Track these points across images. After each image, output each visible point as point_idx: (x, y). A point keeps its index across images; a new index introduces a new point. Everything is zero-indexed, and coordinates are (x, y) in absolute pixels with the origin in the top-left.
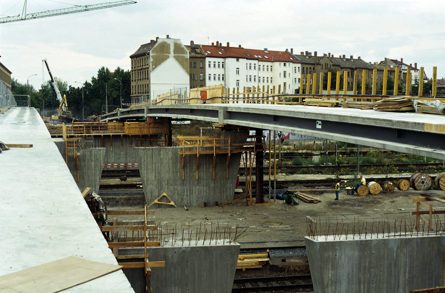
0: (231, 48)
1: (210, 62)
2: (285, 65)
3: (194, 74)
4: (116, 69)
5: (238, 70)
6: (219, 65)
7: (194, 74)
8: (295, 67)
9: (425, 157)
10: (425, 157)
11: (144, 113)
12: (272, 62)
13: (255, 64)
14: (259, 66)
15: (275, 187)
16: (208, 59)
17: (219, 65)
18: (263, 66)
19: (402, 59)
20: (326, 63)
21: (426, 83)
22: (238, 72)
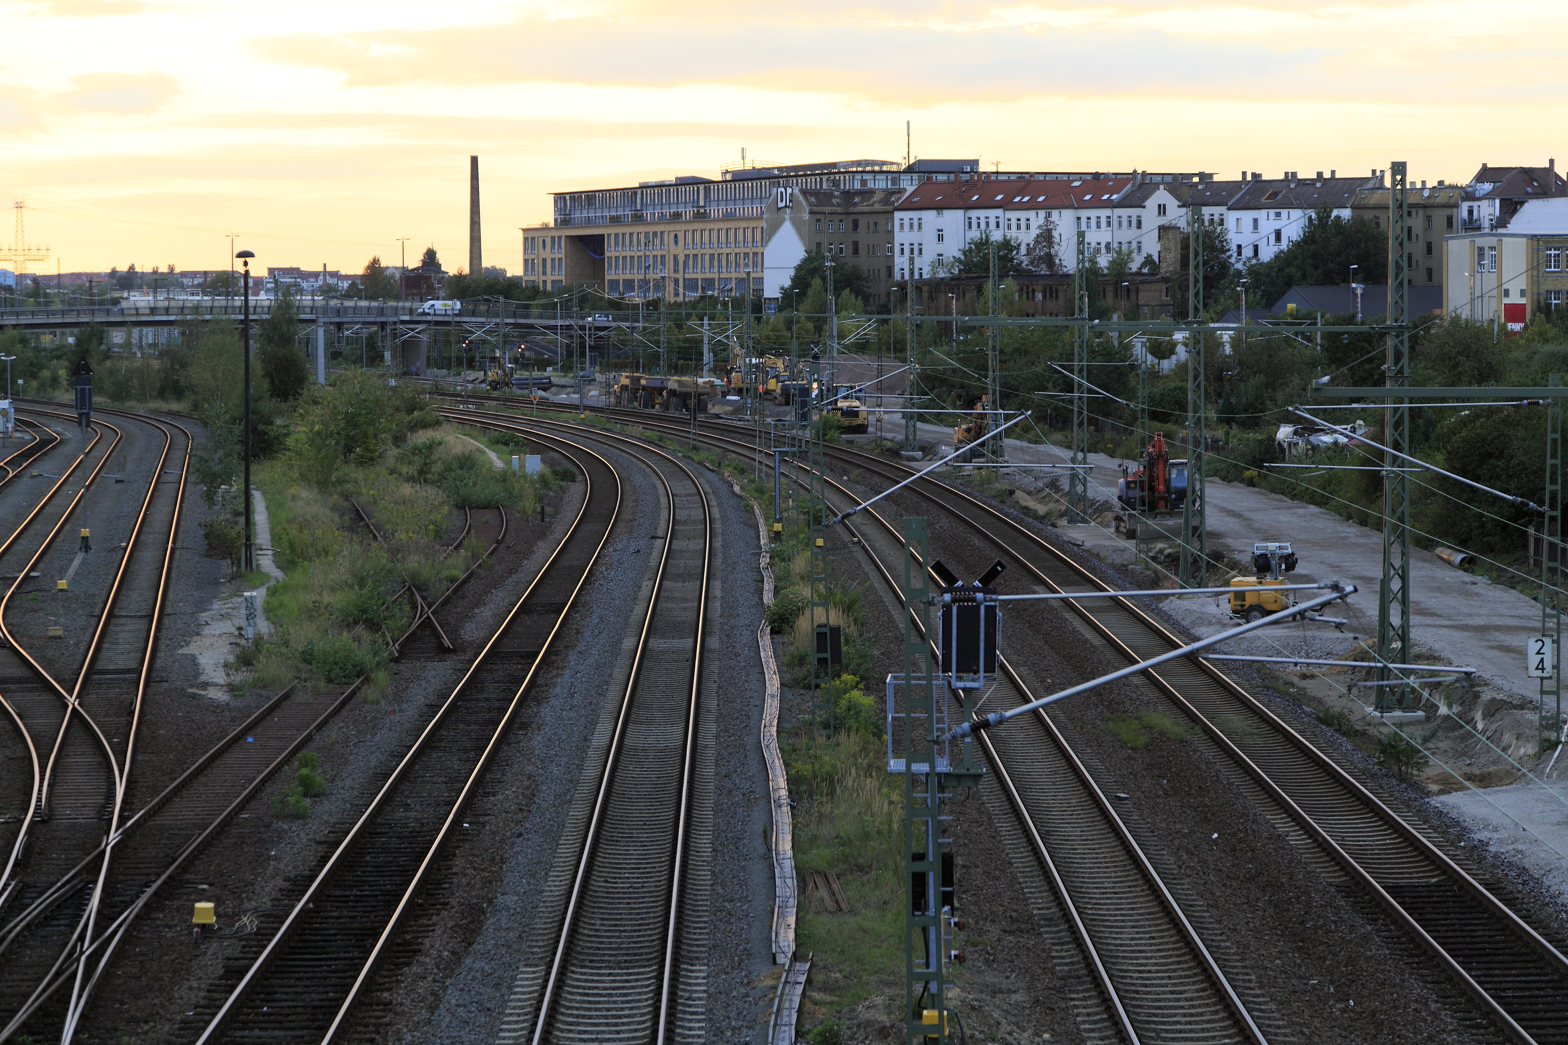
0: (1265, 181)
2: (1278, 215)
5: (1486, 250)
6: (911, 225)
8: (1019, 220)
9: (1041, 710)
10: (1041, 710)
11: (1550, 560)
13: (997, 217)
14: (1009, 220)
16: (898, 215)
17: (911, 225)
18: (1089, 218)
19: (1552, 161)
22: (940, 238)
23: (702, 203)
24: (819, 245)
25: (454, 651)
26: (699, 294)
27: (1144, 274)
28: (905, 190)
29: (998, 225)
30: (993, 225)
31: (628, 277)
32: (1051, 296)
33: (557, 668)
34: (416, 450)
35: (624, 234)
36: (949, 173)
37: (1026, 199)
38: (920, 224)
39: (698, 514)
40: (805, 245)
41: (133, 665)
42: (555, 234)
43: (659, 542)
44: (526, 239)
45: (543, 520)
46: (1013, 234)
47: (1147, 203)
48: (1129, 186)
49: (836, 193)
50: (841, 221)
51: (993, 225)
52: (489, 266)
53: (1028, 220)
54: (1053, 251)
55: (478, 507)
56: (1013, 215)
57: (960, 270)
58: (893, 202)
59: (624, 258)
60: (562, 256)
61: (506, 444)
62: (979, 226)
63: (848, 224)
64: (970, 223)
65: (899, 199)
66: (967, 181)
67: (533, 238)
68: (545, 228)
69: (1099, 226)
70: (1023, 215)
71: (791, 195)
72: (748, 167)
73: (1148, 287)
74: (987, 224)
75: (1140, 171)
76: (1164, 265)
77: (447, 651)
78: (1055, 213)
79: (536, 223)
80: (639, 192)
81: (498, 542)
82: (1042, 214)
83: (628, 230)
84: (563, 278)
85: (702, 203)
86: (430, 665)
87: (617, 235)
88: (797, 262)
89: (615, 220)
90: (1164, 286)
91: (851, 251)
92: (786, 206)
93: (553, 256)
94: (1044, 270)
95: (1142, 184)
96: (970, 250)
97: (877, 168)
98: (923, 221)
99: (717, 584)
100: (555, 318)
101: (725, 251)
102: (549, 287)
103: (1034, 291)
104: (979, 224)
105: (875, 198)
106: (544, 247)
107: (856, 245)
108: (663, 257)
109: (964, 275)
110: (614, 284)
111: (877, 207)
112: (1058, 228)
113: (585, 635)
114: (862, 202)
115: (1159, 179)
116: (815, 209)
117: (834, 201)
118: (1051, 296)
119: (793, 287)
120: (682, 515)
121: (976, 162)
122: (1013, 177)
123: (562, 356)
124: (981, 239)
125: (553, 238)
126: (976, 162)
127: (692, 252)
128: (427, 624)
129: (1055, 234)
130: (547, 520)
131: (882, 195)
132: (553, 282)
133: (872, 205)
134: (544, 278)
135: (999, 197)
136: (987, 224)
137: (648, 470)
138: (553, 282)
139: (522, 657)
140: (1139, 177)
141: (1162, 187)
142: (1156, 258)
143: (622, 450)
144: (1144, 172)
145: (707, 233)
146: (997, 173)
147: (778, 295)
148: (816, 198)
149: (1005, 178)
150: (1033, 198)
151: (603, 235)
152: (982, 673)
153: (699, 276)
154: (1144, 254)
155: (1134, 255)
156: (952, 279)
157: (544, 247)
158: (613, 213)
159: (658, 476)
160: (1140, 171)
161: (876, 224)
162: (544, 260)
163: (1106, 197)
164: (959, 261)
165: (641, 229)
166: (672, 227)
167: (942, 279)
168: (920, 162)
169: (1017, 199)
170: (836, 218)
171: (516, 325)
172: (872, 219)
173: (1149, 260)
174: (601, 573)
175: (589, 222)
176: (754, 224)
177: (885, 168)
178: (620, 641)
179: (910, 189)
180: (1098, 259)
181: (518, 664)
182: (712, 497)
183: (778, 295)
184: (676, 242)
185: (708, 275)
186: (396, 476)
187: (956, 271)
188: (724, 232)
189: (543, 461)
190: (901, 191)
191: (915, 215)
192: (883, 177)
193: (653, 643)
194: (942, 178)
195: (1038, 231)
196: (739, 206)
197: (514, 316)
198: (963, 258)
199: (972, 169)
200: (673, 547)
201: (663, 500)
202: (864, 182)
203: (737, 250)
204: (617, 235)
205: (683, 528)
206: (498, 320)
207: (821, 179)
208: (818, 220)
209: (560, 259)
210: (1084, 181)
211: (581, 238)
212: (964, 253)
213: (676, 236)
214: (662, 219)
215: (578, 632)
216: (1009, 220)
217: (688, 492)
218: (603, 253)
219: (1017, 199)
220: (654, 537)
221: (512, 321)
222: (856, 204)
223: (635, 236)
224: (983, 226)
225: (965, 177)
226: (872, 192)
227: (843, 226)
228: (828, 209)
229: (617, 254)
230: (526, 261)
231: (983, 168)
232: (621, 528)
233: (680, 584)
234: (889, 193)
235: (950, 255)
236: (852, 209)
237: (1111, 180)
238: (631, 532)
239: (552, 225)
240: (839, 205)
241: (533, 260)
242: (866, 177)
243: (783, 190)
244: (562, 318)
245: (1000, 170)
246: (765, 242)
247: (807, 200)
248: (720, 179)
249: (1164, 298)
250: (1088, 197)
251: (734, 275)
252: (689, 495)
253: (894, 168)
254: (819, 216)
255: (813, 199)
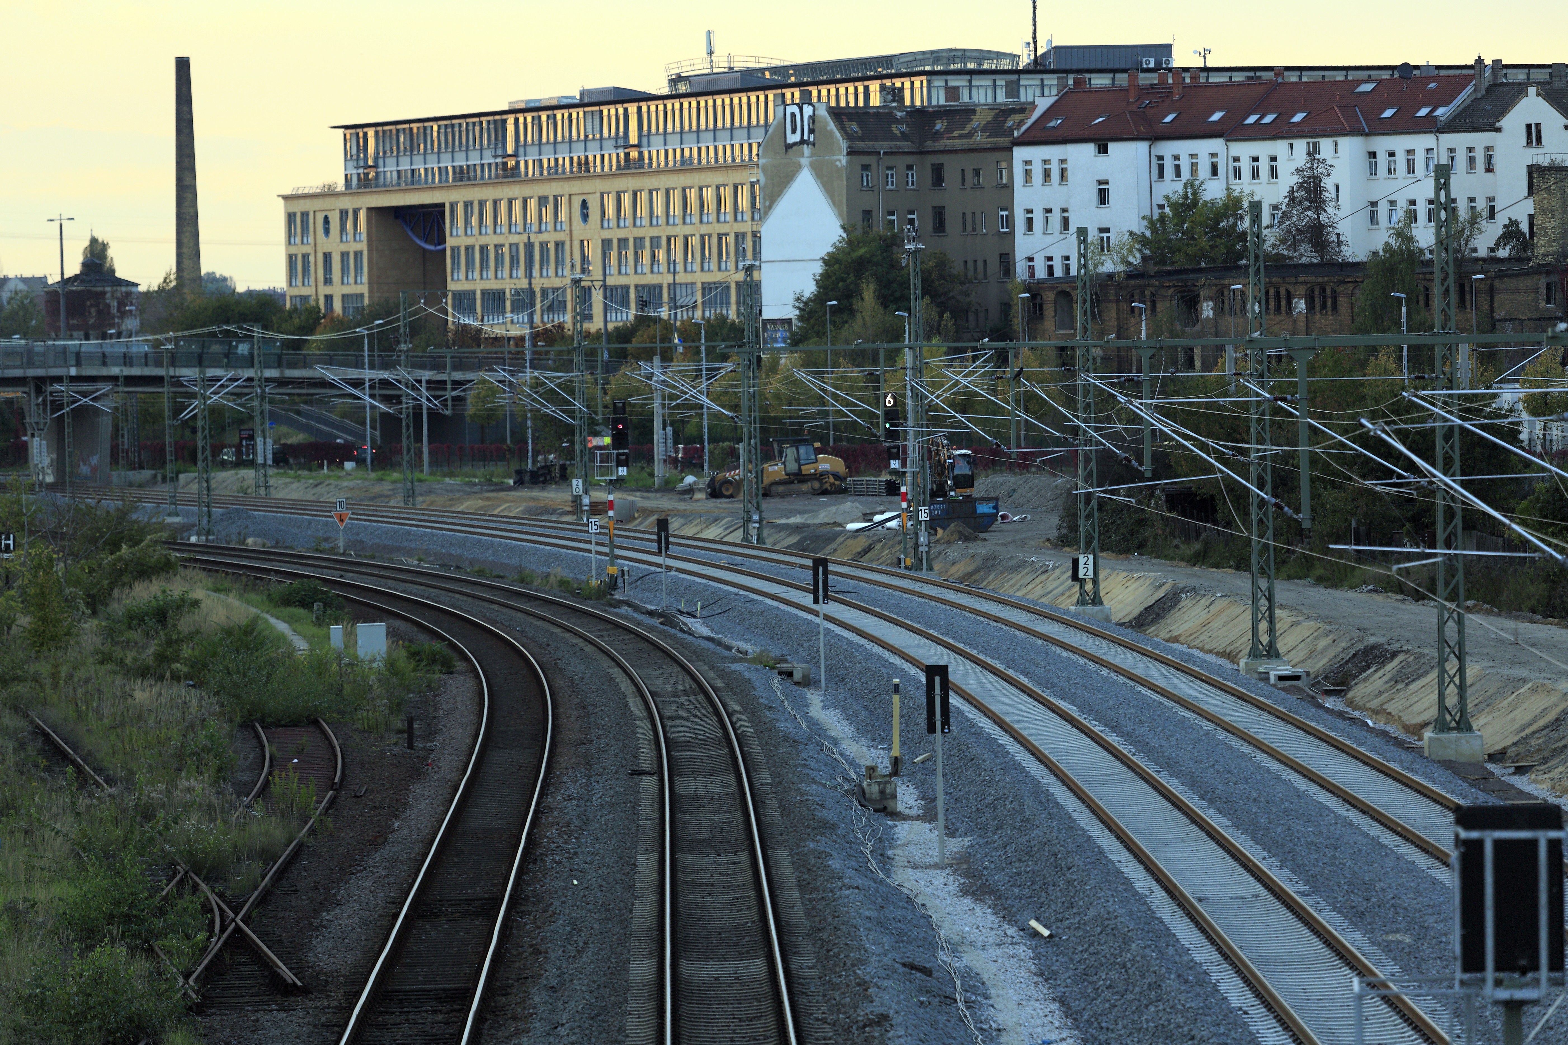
1: (1027, 163)
3: (974, 213)
4: (87, 243)
6: (1047, 174)
7: (974, 213)
8: (1255, 159)
12: (1367, 135)
13: (1213, 155)
14: (1237, 159)
15: (706, 437)
16: (1020, 154)
17: (1047, 174)
18: (1392, 154)
20: (1533, 122)
21: (1213, 202)
22: (1103, 197)
23: (633, 139)
24: (867, 214)
25: (304, 991)
26: (632, 313)
27: (1501, 260)
28: (1033, 105)
29: (1215, 171)
30: (1204, 171)
31: (492, 284)
32: (1324, 306)
33: (515, 1018)
34: (135, 619)
35: (482, 204)
36: (1114, 71)
37: (1268, 119)
38: (1063, 171)
39: (708, 728)
40: (840, 215)
41: (685, 858)
42: (347, 203)
43: (648, 783)
44: (291, 218)
45: (411, 746)
46: (1245, 186)
47: (1504, 123)
48: (1469, 89)
49: (899, 114)
50: (910, 167)
51: (1204, 171)
52: (220, 271)
53: (1274, 159)
54: (1323, 218)
55: (278, 724)
56: (1244, 150)
57: (1145, 259)
58: (1011, 131)
59: (483, 249)
60: (363, 246)
61: (305, 603)
62: (1178, 173)
63: (921, 176)
64: (1161, 168)
65: (1021, 123)
66: (1153, 86)
67: (305, 215)
68: (329, 193)
69: (1411, 168)
70: (1263, 149)
71: (812, 118)
72: (721, 66)
73: (1511, 283)
74: (1194, 167)
75: (1488, 62)
76: (1540, 241)
77: (289, 990)
78: (1326, 145)
79: (312, 182)
80: (511, 119)
81: (338, 788)
82: (1301, 146)
83: (488, 194)
84: (364, 289)
85: (633, 139)
86: (265, 1018)
87: (468, 205)
88: (825, 248)
89: (463, 176)
90: (1543, 281)
91: (929, 226)
92: (803, 142)
93: (344, 247)
94: (1306, 255)
95: (1493, 87)
96: (1162, 218)
97: (971, 66)
98: (1068, 165)
99: (782, 856)
100: (359, 365)
101: (681, 230)
102: (338, 306)
103: (1289, 297)
104: (1178, 168)
105: (977, 121)
106: (327, 231)
107: (939, 215)
108: (559, 245)
109: (1153, 269)
110: (464, 301)
111: (979, 137)
112: (1334, 172)
113: (553, 955)
114: (949, 130)
115: (1521, 76)
116: (860, 145)
117: (895, 129)
118: (1324, 306)
119: (820, 298)
120: (681, 731)
121: (1166, 50)
122: (1238, 77)
123: (373, 440)
124: (1186, 197)
125: (343, 213)
126: (1166, 50)
127: (614, 235)
128: (238, 940)
129: (1328, 183)
130: (418, 744)
131: (989, 116)
132: (344, 297)
133: (970, 135)
134: (328, 290)
135: (1216, 117)
136: (1194, 167)
137: (589, 649)
138: (344, 297)
139: (438, 999)
140: (1488, 72)
141: (1532, 90)
142: (1525, 227)
143: (529, 613)
144: (1497, 62)
145: (644, 196)
146: (1206, 69)
147: (790, 312)
148: (860, 124)
149: (1222, 78)
150: (1283, 117)
151: (442, 205)
152: (1544, 972)
153: (631, 280)
154: (1502, 219)
155: (1483, 223)
156: (1130, 276)
157: (327, 231)
158: (460, 161)
159: (613, 658)
160: (1488, 62)
161: (977, 172)
162: (327, 256)
163: (1423, 112)
164: (1141, 240)
165: (515, 191)
166: (576, 187)
167: (1110, 276)
168: (1059, 51)
169: (1251, 120)
170: (901, 162)
171: (282, 382)
172: (969, 162)
173: (1511, 232)
174: (551, 840)
175: (412, 181)
176: (736, 177)
177: (986, 66)
178: (623, 967)
179: (1043, 104)
180: (1415, 232)
181: (435, 1012)
182: (729, 696)
183: (790, 312)
184: (585, 217)
185: (649, 279)
186: (109, 667)
187: (1136, 259)
188: (678, 194)
189: (391, 633)
190: (1025, 109)
191: (1053, 153)
192: (987, 81)
193: (688, 968)
194: (1100, 81)
195: (1295, 180)
196: (707, 141)
197: (279, 365)
198: (1148, 234)
199: (1158, 64)
200: (678, 790)
201: (635, 704)
202: (952, 93)
203: (704, 229)
204: (468, 205)
205: (687, 754)
206: (249, 373)
207: (866, 89)
208: (866, 167)
209: (358, 254)
210: (1380, 82)
211: (398, 212)
212: (1152, 225)
213: (584, 204)
214: (555, 174)
215: (537, 952)
216: (1237, 159)
217: (679, 687)
218: (442, 240)
219: (1251, 120)
220: (637, 773)
221: (272, 373)
222: (937, 136)
223: (504, 205)
224: (1186, 173)
225: (1145, 79)
226: (968, 112)
227: (914, 176)
228: (883, 146)
229: (469, 241)
230: (291, 260)
231: (1182, 59)
232: (565, 759)
233: (712, 858)
234: (1004, 113)
235: (1125, 229)
236: (930, 145)
237: (1430, 79)
238: (589, 765)
239: (341, 186)
240: (904, 136)
241: (305, 257)
242: (954, 82)
243: (796, 110)
244: (372, 367)
245: (1209, 65)
246: (760, 213)
247: (842, 128)
248: (665, 91)
249: (1543, 304)
250: (1388, 113)
251: (700, 278)
252: (684, 693)
253: (1006, 64)
254: (866, 160)
255: (855, 126)
